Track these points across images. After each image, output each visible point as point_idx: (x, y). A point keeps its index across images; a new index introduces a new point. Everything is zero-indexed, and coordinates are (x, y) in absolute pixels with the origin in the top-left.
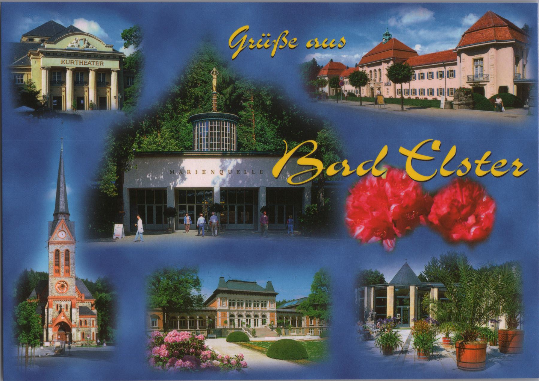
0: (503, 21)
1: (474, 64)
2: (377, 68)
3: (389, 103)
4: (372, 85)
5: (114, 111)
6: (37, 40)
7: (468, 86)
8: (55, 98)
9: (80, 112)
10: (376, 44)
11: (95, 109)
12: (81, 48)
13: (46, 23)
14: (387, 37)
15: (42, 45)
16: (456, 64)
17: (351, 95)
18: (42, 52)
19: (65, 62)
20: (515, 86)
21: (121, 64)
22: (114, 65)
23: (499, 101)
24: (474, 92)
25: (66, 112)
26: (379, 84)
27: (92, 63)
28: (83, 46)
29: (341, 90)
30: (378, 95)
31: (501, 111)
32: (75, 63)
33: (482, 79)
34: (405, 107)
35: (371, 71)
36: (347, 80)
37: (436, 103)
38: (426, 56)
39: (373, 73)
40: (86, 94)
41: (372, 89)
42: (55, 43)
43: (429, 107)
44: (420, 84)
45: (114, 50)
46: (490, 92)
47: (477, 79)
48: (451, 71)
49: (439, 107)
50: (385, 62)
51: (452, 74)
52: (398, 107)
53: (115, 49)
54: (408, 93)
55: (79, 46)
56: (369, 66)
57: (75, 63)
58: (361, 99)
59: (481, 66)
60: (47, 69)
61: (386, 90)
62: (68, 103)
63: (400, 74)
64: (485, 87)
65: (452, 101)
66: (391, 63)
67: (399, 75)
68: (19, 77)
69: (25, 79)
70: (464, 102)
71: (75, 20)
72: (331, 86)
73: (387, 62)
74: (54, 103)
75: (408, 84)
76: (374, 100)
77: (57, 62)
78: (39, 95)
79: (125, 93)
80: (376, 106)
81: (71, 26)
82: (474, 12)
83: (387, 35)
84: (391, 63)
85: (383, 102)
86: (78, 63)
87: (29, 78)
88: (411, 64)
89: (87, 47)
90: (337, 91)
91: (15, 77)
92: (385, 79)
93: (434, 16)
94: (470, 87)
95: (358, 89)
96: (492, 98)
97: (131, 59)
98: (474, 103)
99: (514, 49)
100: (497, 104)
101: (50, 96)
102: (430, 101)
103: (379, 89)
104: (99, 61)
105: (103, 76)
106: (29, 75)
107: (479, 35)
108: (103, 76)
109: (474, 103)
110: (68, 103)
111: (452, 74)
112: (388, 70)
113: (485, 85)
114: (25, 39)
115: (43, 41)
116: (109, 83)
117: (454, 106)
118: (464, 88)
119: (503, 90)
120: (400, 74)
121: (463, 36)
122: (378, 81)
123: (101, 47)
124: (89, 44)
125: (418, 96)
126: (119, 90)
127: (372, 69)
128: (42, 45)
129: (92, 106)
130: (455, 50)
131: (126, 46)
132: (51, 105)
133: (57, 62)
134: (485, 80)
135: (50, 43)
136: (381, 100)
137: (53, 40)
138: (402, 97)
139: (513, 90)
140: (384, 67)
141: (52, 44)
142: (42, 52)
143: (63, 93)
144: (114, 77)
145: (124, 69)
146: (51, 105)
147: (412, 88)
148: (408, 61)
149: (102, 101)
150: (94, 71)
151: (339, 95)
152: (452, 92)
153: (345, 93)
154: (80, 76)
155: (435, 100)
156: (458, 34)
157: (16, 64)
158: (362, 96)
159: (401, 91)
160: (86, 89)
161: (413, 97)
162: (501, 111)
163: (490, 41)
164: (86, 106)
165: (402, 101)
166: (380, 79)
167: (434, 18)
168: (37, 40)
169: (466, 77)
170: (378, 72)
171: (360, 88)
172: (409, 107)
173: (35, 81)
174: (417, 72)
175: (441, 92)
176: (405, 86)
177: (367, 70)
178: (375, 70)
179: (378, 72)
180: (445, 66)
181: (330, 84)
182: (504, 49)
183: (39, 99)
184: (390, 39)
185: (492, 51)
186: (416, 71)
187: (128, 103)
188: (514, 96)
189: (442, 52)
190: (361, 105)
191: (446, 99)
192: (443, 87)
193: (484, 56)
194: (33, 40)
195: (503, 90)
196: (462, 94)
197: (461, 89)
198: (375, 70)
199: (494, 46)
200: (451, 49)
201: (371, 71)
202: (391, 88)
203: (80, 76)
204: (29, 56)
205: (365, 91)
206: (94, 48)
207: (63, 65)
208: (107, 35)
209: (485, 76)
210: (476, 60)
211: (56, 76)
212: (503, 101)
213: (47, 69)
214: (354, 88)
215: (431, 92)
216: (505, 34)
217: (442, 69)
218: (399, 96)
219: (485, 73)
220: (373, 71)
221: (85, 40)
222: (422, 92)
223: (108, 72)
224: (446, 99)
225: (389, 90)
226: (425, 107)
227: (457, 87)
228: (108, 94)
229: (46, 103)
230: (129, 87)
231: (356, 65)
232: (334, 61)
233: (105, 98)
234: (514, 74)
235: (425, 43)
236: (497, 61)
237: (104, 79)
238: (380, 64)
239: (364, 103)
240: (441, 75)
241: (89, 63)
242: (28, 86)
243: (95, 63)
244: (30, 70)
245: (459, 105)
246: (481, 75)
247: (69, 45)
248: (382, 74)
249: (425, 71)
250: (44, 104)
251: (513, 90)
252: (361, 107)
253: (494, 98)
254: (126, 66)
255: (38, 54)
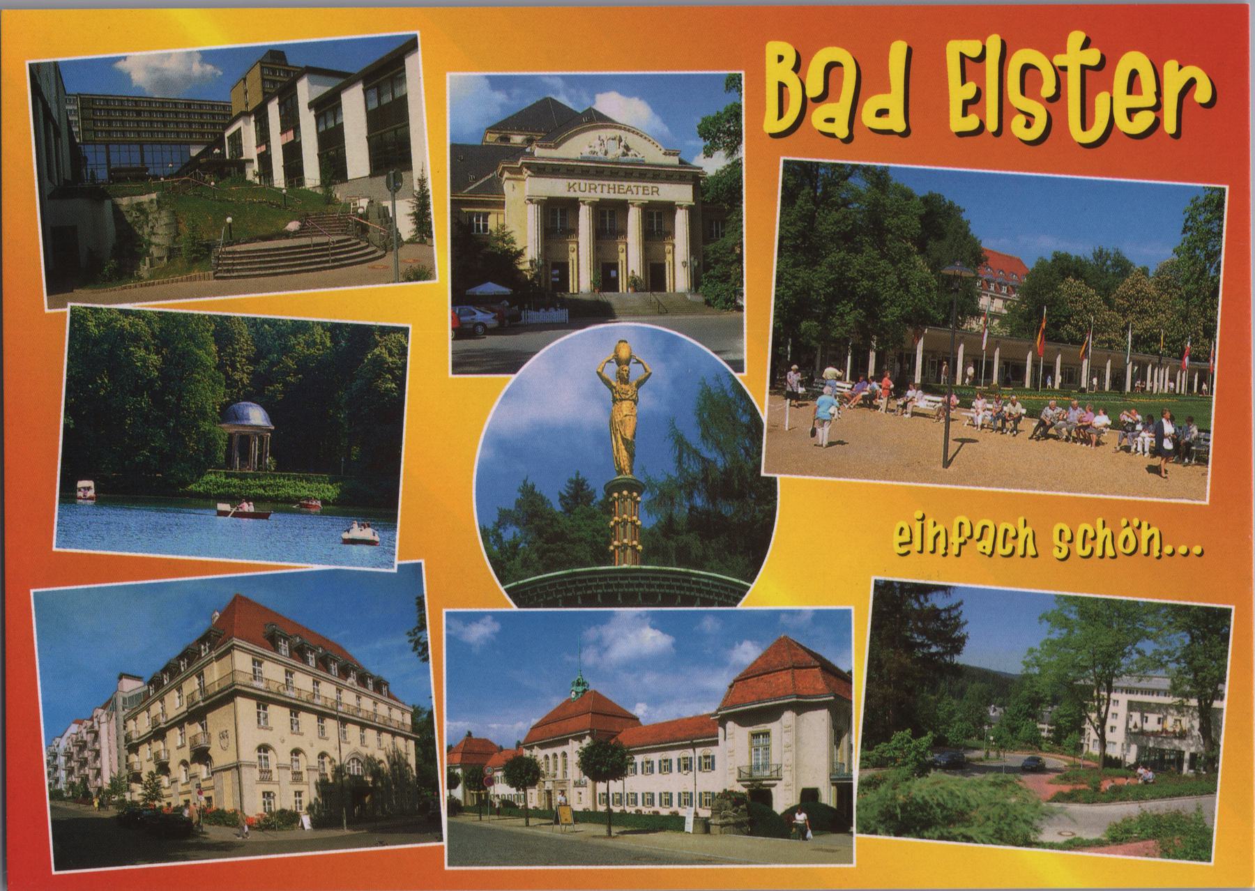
0: (809, 658)
1: (751, 743)
2: (559, 750)
3: (584, 822)
4: (549, 785)
5: (683, 295)
6: (517, 139)
7: (740, 788)
8: (556, 266)
9: (608, 296)
10: (556, 702)
11: (642, 291)
12: (610, 157)
13: (538, 103)
14: (580, 689)
15: (528, 150)
16: (716, 743)
17: (508, 807)
18: (529, 166)
19: (576, 187)
20: (834, 788)
21: (698, 192)
22: (682, 194)
23: (801, 818)
24: (753, 799)
25: (579, 297)
26: (563, 782)
27: (635, 190)
28: (615, 152)
29: (487, 795)
30: (561, 804)
31: (805, 839)
32: (599, 189)
33: (767, 773)
34: (615, 830)
35: (547, 757)
36: (500, 774)
37: (675, 823)
38: (655, 726)
39: (551, 761)
40: (622, 256)
41: (549, 792)
42: (556, 146)
43: (662, 829)
44: (643, 784)
45: (681, 162)
46: (783, 799)
47: (756, 774)
48: (707, 757)
49: (683, 829)
50: (575, 738)
51: (709, 764)
52: (602, 830)
53: (685, 159)
54: (620, 802)
55: (606, 153)
56: (542, 746)
57: (599, 189)
58: (527, 813)
59: (767, 748)
60: (538, 203)
61: (576, 795)
62: (583, 281)
63: (605, 762)
64: (773, 790)
65: (708, 819)
66: (587, 741)
67: (602, 764)
68: (478, 220)
69: (492, 223)
70: (732, 820)
71: (599, 97)
72: (468, 786)
73: (580, 738)
74: (554, 276)
75: (620, 782)
76: (551, 815)
77: (558, 188)
78: (522, 259)
79: (706, 256)
80: (557, 827)
81: (590, 109)
82: (752, 638)
83: (578, 684)
84: (587, 741)
85: (571, 820)
86: (606, 189)
87: (501, 222)
88: (626, 743)
89: (625, 155)
90: (479, 796)
91: (471, 219)
92: (575, 773)
93: (674, 645)
94: (745, 790)
95: (521, 792)
96: (787, 812)
97: (719, 182)
98: (751, 823)
99: (831, 714)
100: (797, 825)
101: (545, 261)
102: (665, 817)
103: (563, 793)
104: (650, 185)
105: (657, 219)
106: (501, 217)
107: (762, 684)
108: (657, 219)
109: (751, 823)
110: (583, 281)
111: (709, 764)
112: (580, 754)
113: (774, 785)
114: (492, 138)
115: (530, 141)
116: (671, 233)
117: (712, 828)
118: (731, 792)
119: (810, 796)
120: (605, 762)
121: (731, 687)
122: (560, 777)
123: (653, 155)
124: (627, 148)
125: (640, 806)
126: (694, 250)
127: (549, 752)
128: (528, 150)
129: (635, 284)
130: (716, 714)
131: (708, 153)
132: (547, 281)
133: (558, 188)
134: (775, 775)
135: (546, 147)
136: (566, 815)
137: (550, 140)
138: (609, 810)
139: (828, 797)
140: (573, 749)
141: (550, 147)
142: (529, 166)
143: (573, 256)
144: (681, 219)
145: (704, 202)
146: (547, 281)
147: (627, 791)
148: (620, 737)
149: (655, 275)
150: (639, 206)
151: (484, 805)
152: (710, 799)
153: (496, 801)
154: (609, 219)
155: (675, 815)
156: (720, 682)
157: (470, 192)
158: (530, 806)
159: (606, 798)
160: (621, 247)
161: (630, 809)
162: (805, 839)
163: (785, 697)
164: (623, 284)
165: (608, 818)
166: (565, 773)
167: (673, 651)
168: (517, 139)
169: (736, 771)
170: (560, 759)
171: (525, 790)
172: (623, 829)
173: (512, 226)
174: (639, 759)
175: (686, 799)
176: (615, 786)
177: (539, 754)
178: (555, 755)
179: (560, 759)
180: (694, 746)
181: (465, 783)
182: (812, 713)
183: (521, 267)
184: (585, 691)
185: (788, 716)
186: (636, 757)
187: (711, 276)
188: (831, 809)
189: (690, 719)
190: (527, 825)
191: (696, 813)
192: (690, 789)
193: (774, 727)
194: (508, 140)
195: (810, 796)
196: (728, 803)
197: (727, 794)
198: (555, 755)
199: (789, 707)
200: (705, 712)
201: (547, 757)
202: (587, 792)
203: (609, 219)
204: (501, 175)
205: (534, 798)
206: (639, 157)
207: (572, 194)
208: (666, 129)
209: (774, 768)
210: (755, 736)
211: (556, 216)
212: (809, 819)
213: (538, 203)
214: (513, 791)
215: (667, 799)
216: (814, 682)
217: (689, 753)
218: (602, 808)
219: (775, 758)
220: (550, 756)
221: (620, 140)
222: (649, 799)
223: (669, 209)
224: (696, 813)
225: (582, 797)
226: (654, 831)
227: (718, 789)
228: (669, 257)
229: (536, 275)
230: (714, 241)
231: (519, 744)
232: (474, 736)
233: (663, 266)
234: (832, 763)
235: (655, 701)
236: (798, 740)
237: (659, 224)
238: (565, 742)
239: (532, 821)
240: (686, 765)
241: (629, 189)
242: (497, 239)
243: (641, 190)
244: (501, 205)
245: (722, 825)
246: (766, 766)
247: (586, 152)
248: (569, 763)
249: (656, 757)
250: (532, 280)
251: (828, 797)
252: (529, 830)
253: (791, 812)
254: (708, 197)
255: (519, 171)
